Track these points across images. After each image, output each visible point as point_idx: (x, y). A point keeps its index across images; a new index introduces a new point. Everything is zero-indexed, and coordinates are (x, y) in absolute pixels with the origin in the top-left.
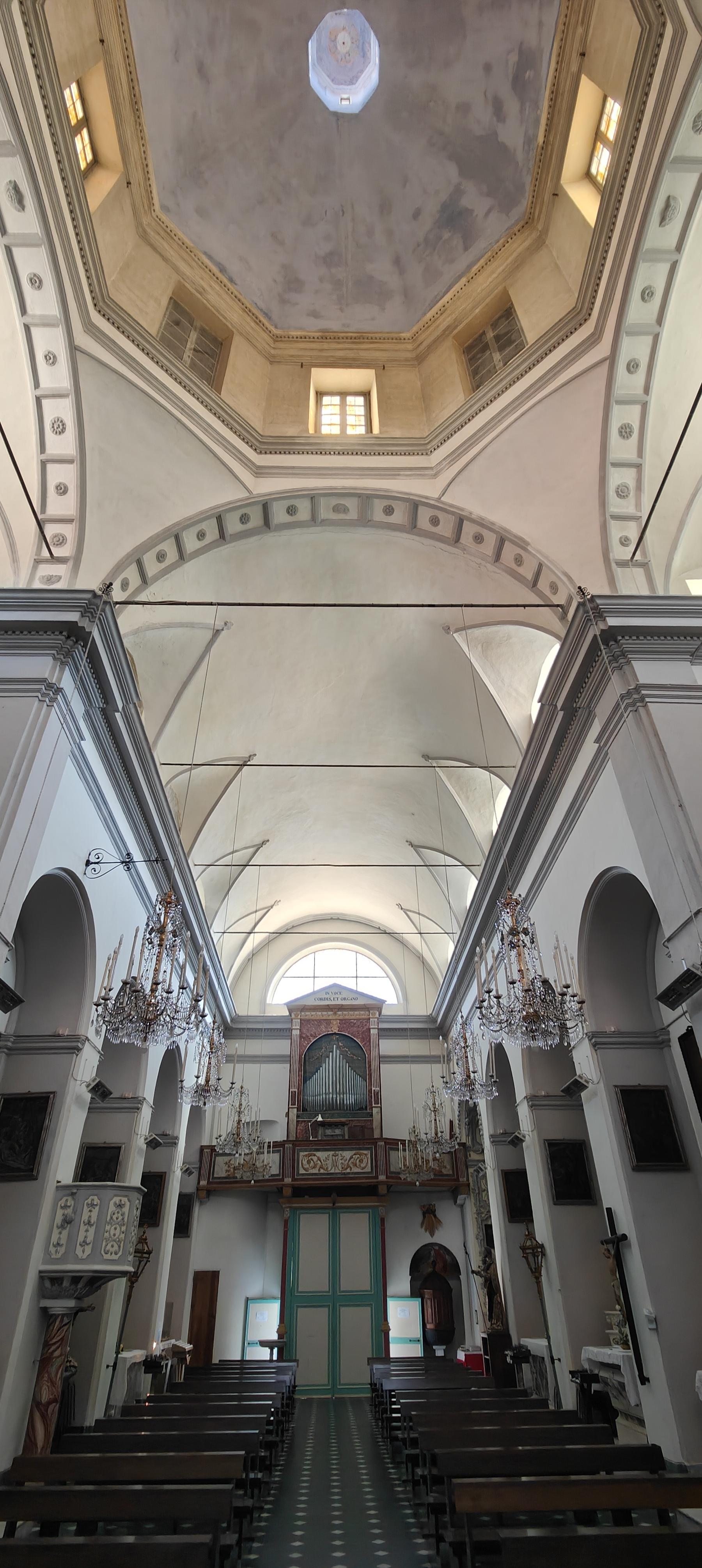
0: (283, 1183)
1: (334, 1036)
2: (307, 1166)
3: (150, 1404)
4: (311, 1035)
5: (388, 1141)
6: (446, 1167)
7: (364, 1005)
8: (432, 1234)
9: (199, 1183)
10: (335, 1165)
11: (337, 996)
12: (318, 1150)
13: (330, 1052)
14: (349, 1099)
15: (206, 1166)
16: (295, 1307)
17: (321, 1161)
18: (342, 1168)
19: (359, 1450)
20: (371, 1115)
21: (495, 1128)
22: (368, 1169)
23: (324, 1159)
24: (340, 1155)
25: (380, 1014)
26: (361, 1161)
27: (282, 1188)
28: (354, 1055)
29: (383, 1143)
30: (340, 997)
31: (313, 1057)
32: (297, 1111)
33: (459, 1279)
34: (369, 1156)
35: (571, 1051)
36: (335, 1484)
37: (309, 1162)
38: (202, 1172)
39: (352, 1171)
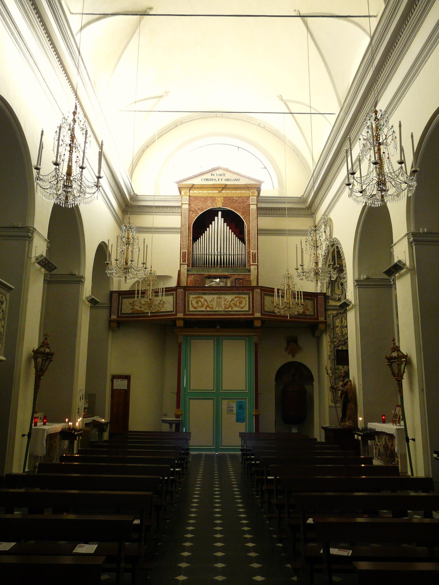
0: (177, 317)
2: (196, 305)
3: (65, 463)
4: (199, 209)
5: (263, 289)
7: (246, 185)
8: (293, 356)
9: (110, 317)
10: (219, 304)
11: (221, 177)
12: (205, 294)
15: (115, 305)
16: (188, 399)
17: (207, 302)
18: (225, 307)
19: (233, 479)
20: (249, 271)
21: (359, 275)
22: (246, 308)
23: (210, 300)
24: (223, 298)
25: (259, 193)
26: (241, 303)
27: (175, 321)
29: (260, 290)
30: (224, 178)
33: (312, 385)
34: (247, 299)
35: (392, 247)
36: (216, 489)
37: (197, 302)
38: (113, 309)
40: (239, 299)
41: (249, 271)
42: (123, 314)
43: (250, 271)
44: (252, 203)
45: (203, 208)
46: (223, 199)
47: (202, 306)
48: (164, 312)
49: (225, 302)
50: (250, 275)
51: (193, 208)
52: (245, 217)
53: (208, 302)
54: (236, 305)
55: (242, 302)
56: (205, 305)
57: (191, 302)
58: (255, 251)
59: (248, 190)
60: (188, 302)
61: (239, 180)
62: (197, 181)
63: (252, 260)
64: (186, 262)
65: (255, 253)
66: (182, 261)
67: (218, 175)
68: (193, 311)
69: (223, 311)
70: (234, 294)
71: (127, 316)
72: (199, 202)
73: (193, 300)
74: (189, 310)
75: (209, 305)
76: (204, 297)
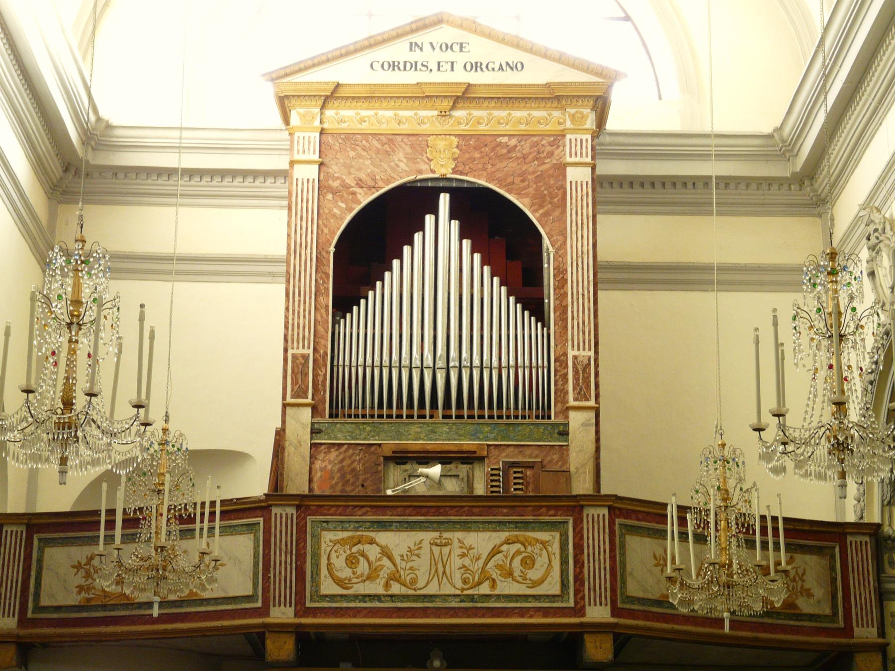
2: (345, 573)
4: (360, 184)
17: (390, 558)
18: (465, 581)
20: (564, 434)
22: (552, 586)
23: (404, 551)
24: (456, 543)
26: (529, 562)
34: (556, 547)
37: (351, 561)
39: (497, 592)
40: (523, 549)
42: (45, 609)
45: (378, 177)
47: (370, 578)
49: (467, 561)
50: (568, 450)
51: (337, 178)
53: (398, 560)
55: (534, 562)
56: (381, 573)
59: (556, 108)
60: (316, 556)
63: (574, 389)
65: (586, 361)
66: (292, 390)
69: (459, 595)
70: (500, 526)
72: (360, 156)
73: (333, 552)
74: (317, 591)
75: (402, 572)
76: (377, 540)
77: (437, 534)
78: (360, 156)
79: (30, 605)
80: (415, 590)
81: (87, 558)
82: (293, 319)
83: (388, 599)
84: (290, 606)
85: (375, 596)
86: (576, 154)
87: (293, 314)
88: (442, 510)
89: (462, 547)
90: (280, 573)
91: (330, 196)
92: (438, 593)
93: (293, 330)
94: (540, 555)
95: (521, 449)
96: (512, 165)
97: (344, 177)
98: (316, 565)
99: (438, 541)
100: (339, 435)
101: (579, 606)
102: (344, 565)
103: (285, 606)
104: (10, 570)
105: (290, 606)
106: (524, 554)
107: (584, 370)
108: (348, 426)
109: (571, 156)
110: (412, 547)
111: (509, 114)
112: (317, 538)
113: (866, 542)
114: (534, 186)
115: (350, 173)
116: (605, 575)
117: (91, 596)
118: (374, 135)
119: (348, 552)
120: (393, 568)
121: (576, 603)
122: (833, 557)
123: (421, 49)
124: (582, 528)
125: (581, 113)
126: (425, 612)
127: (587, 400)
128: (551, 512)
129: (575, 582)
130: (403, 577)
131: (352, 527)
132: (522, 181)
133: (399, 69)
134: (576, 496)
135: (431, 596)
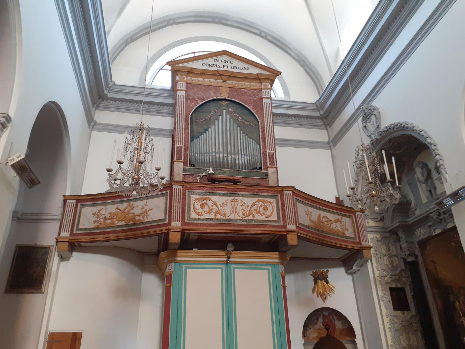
1: (223, 101)
2: (200, 210)
4: (199, 98)
6: (348, 231)
9: (59, 234)
11: (227, 64)
13: (220, 115)
14: (242, 160)
17: (216, 206)
18: (243, 215)
20: (267, 175)
22: (274, 217)
23: (221, 204)
24: (240, 201)
26: (265, 209)
28: (245, 120)
31: (201, 119)
32: (184, 165)
34: (274, 204)
37: (202, 206)
39: (255, 219)
40: (263, 204)
41: (265, 175)
42: (81, 229)
43: (268, 175)
44: (265, 96)
45: (204, 97)
46: (228, 90)
47: (210, 212)
48: (149, 222)
49: (244, 208)
50: (269, 180)
51: (191, 96)
52: (256, 111)
53: (219, 206)
54: (259, 213)
55: (267, 209)
56: (213, 211)
57: (194, 205)
58: (272, 151)
59: (259, 83)
60: (189, 204)
61: (249, 69)
62: (197, 65)
63: (269, 162)
64: (182, 160)
65: (272, 154)
66: (177, 157)
67: (223, 61)
68: (196, 218)
69: (241, 219)
70: (255, 196)
71: (88, 232)
72: (199, 91)
73: (195, 203)
74: (189, 217)
75: (221, 211)
76: (212, 199)
77: (233, 198)
78: (199, 91)
79: (75, 228)
80: (225, 217)
81: (98, 210)
82: (177, 135)
83: (216, 220)
84: (179, 222)
85: (211, 219)
86: (266, 95)
87: (177, 134)
88: (235, 190)
89: (242, 203)
90: (176, 209)
91: (189, 101)
92: (234, 218)
93: (177, 139)
94: (269, 207)
95: (254, 179)
96: (246, 97)
97: (193, 96)
98: (189, 207)
99: (233, 200)
100: (192, 172)
101: (284, 225)
102: (200, 207)
103: (177, 222)
104: (68, 216)
105: (179, 222)
106: (264, 206)
107: (272, 156)
108: (196, 169)
109: (264, 95)
110: (224, 202)
111: (245, 83)
112: (190, 198)
113: (362, 215)
114: (253, 103)
115: (195, 95)
116: (293, 214)
117: (99, 224)
118: (203, 85)
119: (201, 203)
120: (218, 209)
121: (283, 224)
122: (353, 219)
123: (218, 61)
124: (284, 198)
125: (267, 84)
126: (229, 225)
127: (274, 165)
128: (273, 192)
129: (282, 216)
130: (221, 212)
131: (202, 194)
132: (250, 101)
133: (211, 66)
134: (281, 187)
135: (231, 219)
